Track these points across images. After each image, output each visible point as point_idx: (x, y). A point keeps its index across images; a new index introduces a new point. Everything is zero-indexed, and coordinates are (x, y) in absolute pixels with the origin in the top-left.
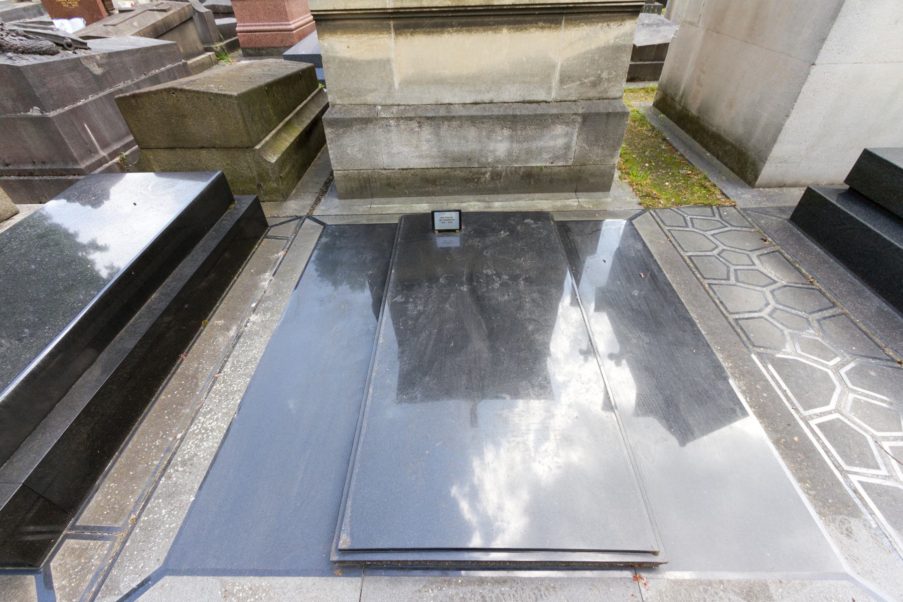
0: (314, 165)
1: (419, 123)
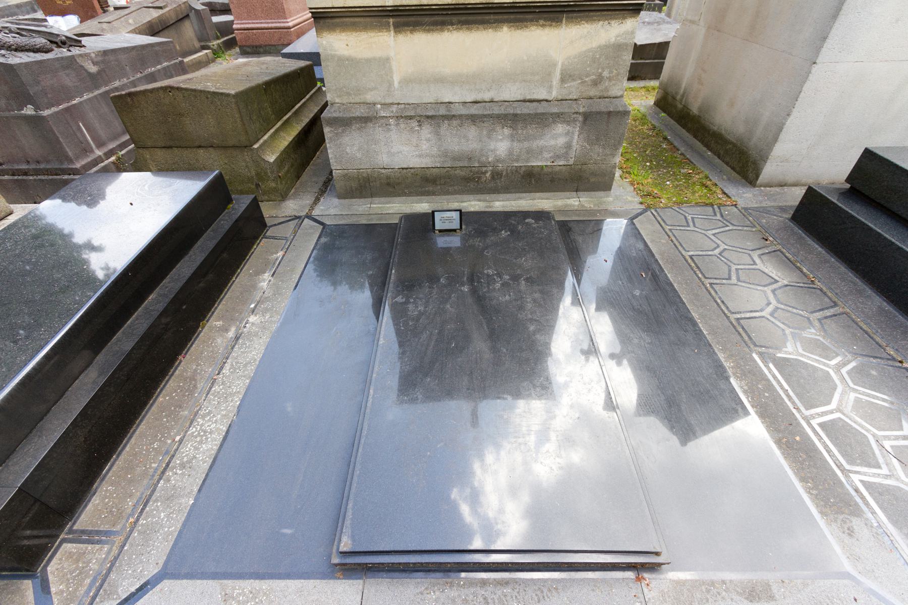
1: (419, 121)
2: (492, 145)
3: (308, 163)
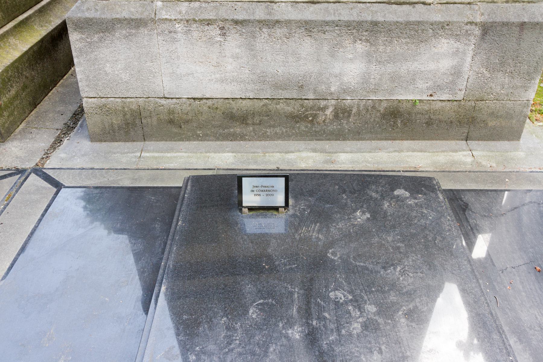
0: (62, 86)
1: (222, 28)
2: (337, 67)
3: (54, 83)
